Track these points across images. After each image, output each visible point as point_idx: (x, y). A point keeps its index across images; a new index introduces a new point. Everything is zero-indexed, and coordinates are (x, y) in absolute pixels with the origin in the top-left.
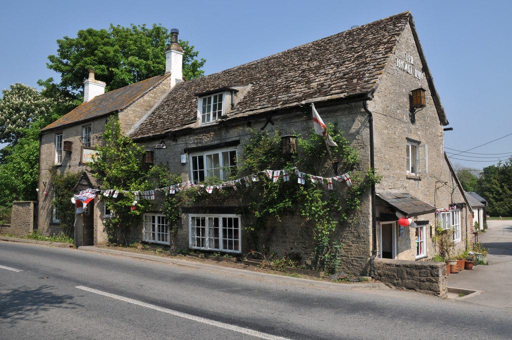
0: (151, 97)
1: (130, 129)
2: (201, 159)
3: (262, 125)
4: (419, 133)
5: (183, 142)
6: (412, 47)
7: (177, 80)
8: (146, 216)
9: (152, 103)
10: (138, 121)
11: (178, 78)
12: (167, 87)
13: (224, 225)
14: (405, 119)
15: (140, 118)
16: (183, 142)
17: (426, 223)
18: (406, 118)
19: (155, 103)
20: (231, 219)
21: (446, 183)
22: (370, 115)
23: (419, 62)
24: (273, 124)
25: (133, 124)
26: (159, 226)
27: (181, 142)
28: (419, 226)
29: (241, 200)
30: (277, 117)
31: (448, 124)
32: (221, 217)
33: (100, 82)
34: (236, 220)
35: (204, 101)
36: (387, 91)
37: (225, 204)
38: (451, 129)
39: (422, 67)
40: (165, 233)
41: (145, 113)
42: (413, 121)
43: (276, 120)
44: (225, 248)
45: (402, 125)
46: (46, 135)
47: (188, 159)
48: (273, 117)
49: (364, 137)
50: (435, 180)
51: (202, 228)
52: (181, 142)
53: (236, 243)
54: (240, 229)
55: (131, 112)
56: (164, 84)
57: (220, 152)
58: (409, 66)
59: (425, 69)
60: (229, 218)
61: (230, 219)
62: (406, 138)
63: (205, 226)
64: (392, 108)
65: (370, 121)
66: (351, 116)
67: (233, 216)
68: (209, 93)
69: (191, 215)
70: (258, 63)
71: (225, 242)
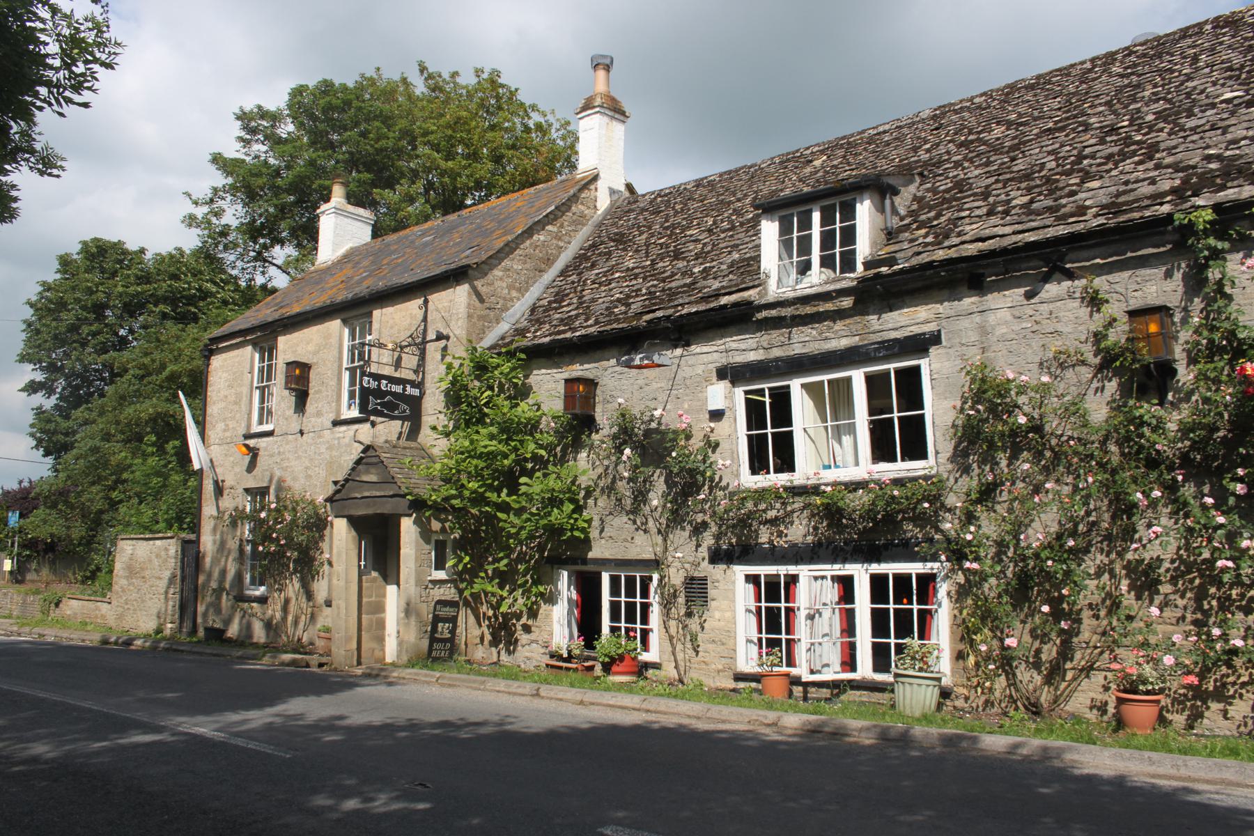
2: (782, 400)
7: (612, 192)
15: (522, 290)
35: (785, 230)
47: (730, 397)
60: (896, 577)
63: (874, 611)
68: (802, 202)
69: (740, 571)
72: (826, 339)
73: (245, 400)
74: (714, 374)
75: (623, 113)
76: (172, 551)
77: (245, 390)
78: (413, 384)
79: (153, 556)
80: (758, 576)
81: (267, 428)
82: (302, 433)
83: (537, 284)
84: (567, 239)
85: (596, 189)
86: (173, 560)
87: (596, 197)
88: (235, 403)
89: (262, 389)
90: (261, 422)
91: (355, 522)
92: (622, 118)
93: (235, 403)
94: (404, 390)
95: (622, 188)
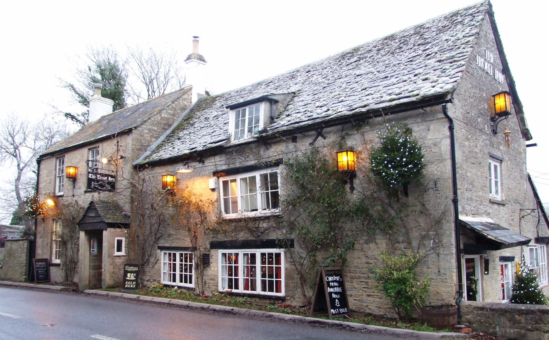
0: (170, 114)
1: (146, 151)
3: (310, 140)
4: (501, 147)
5: (212, 164)
6: (491, 43)
7: (199, 95)
9: (171, 121)
10: (155, 141)
12: (188, 102)
13: (263, 262)
14: (486, 129)
15: (157, 138)
16: (212, 164)
17: (511, 259)
18: (487, 129)
19: (174, 121)
20: (272, 254)
22: (450, 120)
23: (499, 61)
24: (325, 138)
25: (149, 146)
27: (209, 164)
28: (504, 263)
29: (284, 231)
30: (329, 129)
31: (532, 138)
32: (258, 252)
33: (107, 100)
34: (278, 255)
36: (467, 94)
37: (265, 238)
38: (535, 145)
39: (501, 68)
40: (188, 274)
41: (162, 133)
42: (495, 132)
43: (329, 133)
44: (264, 289)
45: (484, 137)
46: (46, 161)
48: (325, 130)
49: (443, 149)
50: (518, 207)
51: (235, 266)
52: (209, 164)
53: (278, 283)
54: (283, 266)
56: (184, 100)
57: (257, 175)
58: (489, 65)
59: (506, 71)
61: (270, 255)
64: (473, 115)
65: (451, 129)
66: (425, 124)
67: (274, 251)
69: (221, 251)
71: (263, 282)
72: (247, 161)
73: (53, 182)
74: (212, 174)
75: (204, 61)
76: (26, 246)
77: (53, 178)
78: (112, 176)
79: (18, 248)
80: (226, 254)
81: (61, 194)
82: (73, 196)
83: (163, 135)
84: (177, 116)
85: (191, 94)
86: (26, 249)
87: (191, 98)
88: (49, 183)
89: (60, 177)
90: (60, 191)
91: (87, 233)
92: (203, 63)
93: (49, 183)
94: (108, 179)
95: (204, 93)
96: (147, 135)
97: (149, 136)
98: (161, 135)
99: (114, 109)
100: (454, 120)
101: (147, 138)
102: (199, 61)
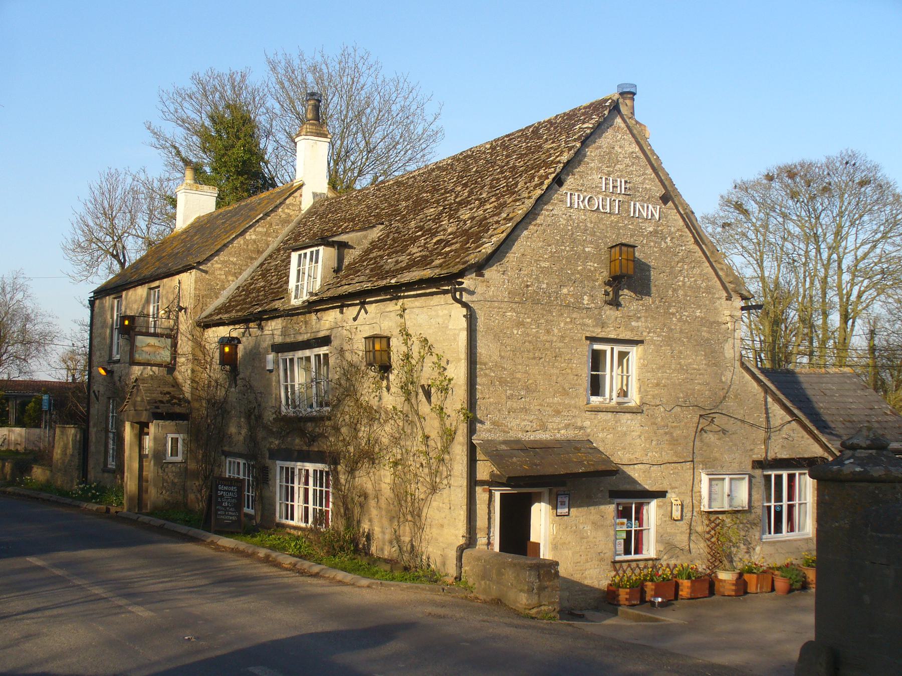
0: (261, 233)
1: (217, 298)
7: (315, 195)
8: (230, 462)
9: (261, 245)
10: (233, 281)
11: (319, 191)
15: (236, 275)
21: (803, 437)
26: (315, 491)
55: (220, 266)
62: (587, 338)
69: (279, 463)
70: (192, 237)
85: (301, 196)
96: (219, 272)
97: (223, 272)
98: (245, 270)
99: (218, 205)
100: (453, 302)
101: (219, 276)
102: (316, 138)
